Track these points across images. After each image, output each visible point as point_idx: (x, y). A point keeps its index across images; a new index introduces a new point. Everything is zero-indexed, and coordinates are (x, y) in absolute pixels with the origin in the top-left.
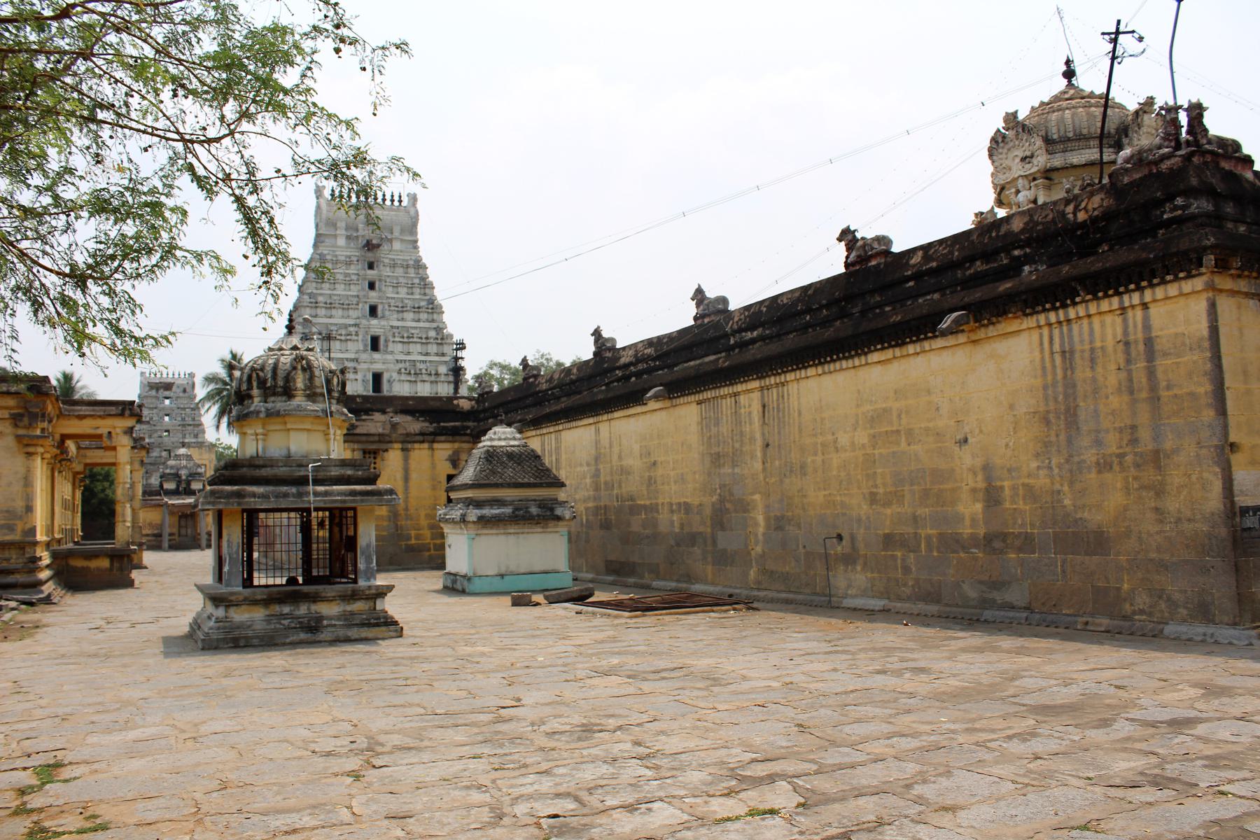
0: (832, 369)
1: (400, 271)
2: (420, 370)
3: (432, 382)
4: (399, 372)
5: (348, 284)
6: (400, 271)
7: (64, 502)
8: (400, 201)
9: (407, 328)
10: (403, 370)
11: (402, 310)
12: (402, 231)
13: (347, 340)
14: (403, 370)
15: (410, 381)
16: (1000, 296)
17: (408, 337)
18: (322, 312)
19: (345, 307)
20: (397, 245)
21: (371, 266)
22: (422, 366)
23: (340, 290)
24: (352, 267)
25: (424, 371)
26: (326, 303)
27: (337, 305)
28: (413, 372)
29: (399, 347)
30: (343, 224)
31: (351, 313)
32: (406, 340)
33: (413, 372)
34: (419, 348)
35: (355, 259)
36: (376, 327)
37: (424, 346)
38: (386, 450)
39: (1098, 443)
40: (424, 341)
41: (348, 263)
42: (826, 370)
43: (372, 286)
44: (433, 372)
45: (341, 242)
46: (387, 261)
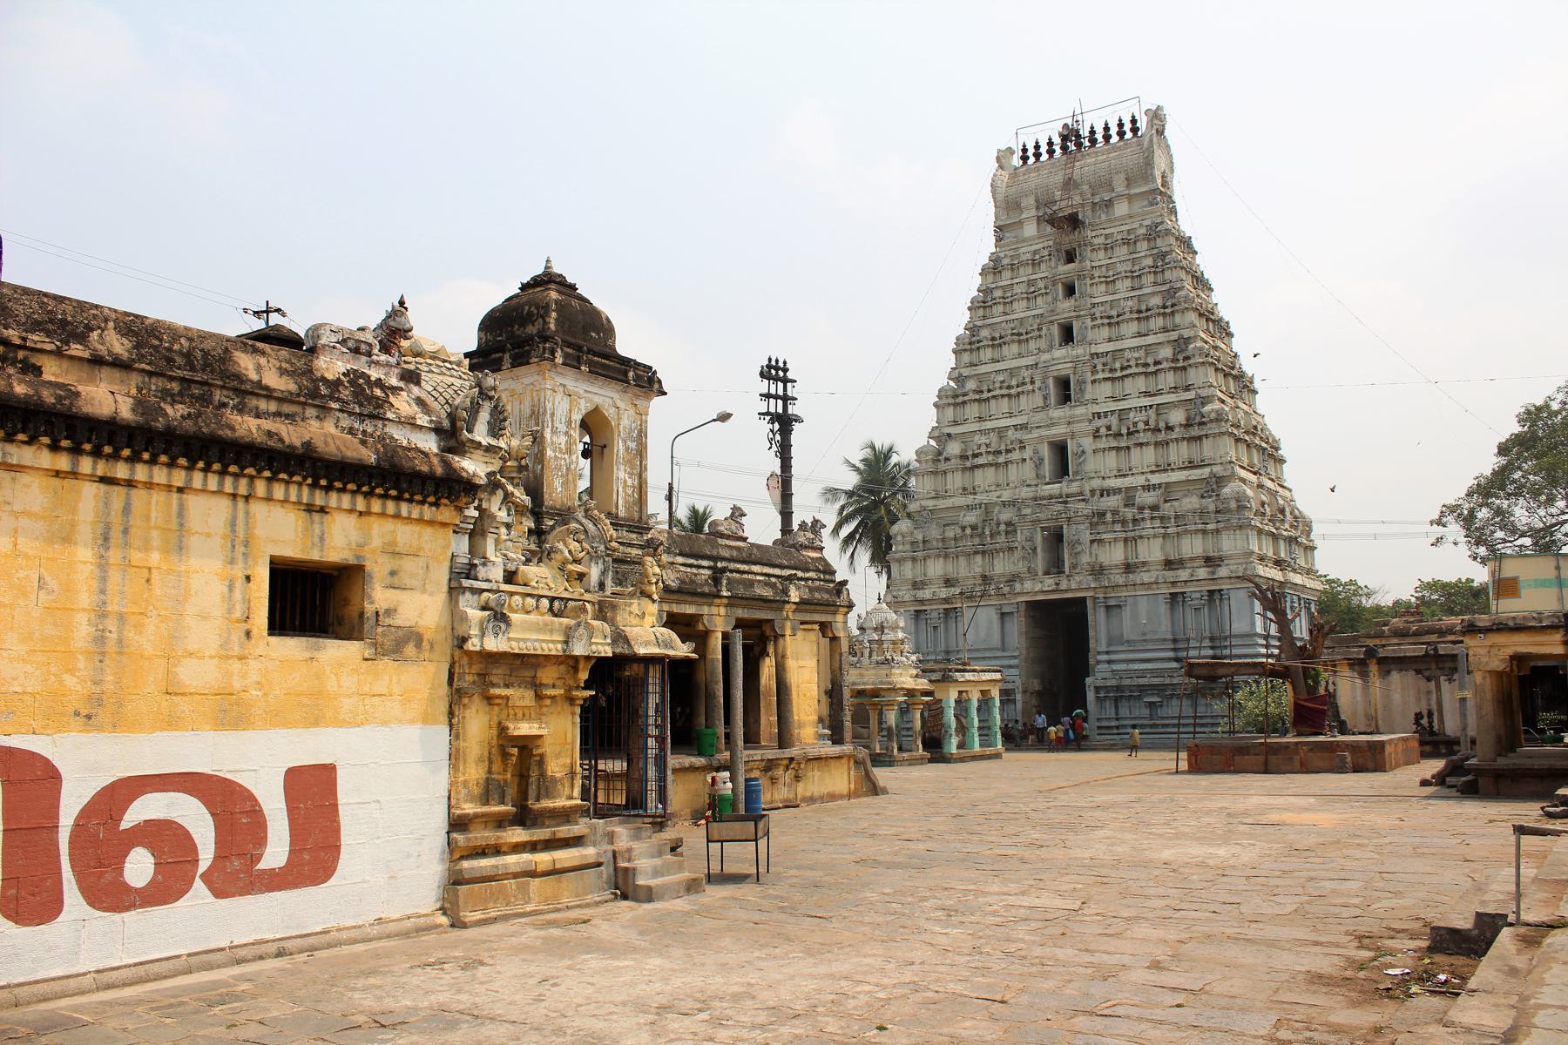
0: (415, 515)
1: (1122, 252)
2: (1135, 424)
3: (1157, 444)
4: (1096, 435)
5: (1031, 297)
6: (1122, 252)
7: (1439, 637)
8: (1135, 130)
9: (1012, 372)
10: (1103, 431)
11: (1113, 322)
12: (1129, 182)
13: (1123, 378)
14: (1103, 431)
15: (1118, 449)
16: (573, 349)
17: (1122, 369)
18: (987, 354)
19: (1021, 338)
20: (1121, 209)
21: (1070, 258)
22: (1141, 417)
23: (1020, 310)
24: (1043, 266)
25: (1141, 426)
26: (993, 339)
27: (1007, 339)
28: (1124, 431)
29: (1106, 389)
30: (1032, 200)
31: (1032, 345)
32: (1118, 374)
33: (1124, 431)
34: (1141, 383)
35: (1046, 253)
36: (1061, 358)
37: (1151, 379)
38: (1220, 566)
39: (1505, 541)
40: (1152, 369)
41: (1035, 263)
42: (404, 513)
43: (1070, 291)
44: (1162, 425)
45: (1030, 230)
46: (1096, 241)
